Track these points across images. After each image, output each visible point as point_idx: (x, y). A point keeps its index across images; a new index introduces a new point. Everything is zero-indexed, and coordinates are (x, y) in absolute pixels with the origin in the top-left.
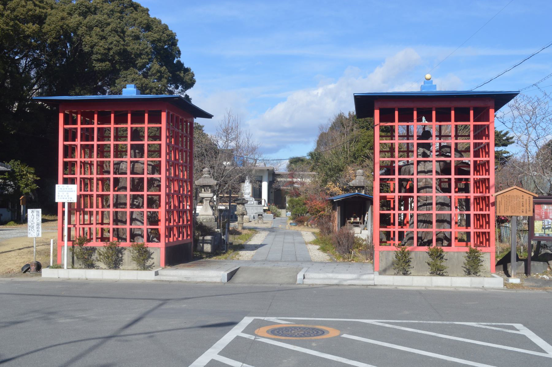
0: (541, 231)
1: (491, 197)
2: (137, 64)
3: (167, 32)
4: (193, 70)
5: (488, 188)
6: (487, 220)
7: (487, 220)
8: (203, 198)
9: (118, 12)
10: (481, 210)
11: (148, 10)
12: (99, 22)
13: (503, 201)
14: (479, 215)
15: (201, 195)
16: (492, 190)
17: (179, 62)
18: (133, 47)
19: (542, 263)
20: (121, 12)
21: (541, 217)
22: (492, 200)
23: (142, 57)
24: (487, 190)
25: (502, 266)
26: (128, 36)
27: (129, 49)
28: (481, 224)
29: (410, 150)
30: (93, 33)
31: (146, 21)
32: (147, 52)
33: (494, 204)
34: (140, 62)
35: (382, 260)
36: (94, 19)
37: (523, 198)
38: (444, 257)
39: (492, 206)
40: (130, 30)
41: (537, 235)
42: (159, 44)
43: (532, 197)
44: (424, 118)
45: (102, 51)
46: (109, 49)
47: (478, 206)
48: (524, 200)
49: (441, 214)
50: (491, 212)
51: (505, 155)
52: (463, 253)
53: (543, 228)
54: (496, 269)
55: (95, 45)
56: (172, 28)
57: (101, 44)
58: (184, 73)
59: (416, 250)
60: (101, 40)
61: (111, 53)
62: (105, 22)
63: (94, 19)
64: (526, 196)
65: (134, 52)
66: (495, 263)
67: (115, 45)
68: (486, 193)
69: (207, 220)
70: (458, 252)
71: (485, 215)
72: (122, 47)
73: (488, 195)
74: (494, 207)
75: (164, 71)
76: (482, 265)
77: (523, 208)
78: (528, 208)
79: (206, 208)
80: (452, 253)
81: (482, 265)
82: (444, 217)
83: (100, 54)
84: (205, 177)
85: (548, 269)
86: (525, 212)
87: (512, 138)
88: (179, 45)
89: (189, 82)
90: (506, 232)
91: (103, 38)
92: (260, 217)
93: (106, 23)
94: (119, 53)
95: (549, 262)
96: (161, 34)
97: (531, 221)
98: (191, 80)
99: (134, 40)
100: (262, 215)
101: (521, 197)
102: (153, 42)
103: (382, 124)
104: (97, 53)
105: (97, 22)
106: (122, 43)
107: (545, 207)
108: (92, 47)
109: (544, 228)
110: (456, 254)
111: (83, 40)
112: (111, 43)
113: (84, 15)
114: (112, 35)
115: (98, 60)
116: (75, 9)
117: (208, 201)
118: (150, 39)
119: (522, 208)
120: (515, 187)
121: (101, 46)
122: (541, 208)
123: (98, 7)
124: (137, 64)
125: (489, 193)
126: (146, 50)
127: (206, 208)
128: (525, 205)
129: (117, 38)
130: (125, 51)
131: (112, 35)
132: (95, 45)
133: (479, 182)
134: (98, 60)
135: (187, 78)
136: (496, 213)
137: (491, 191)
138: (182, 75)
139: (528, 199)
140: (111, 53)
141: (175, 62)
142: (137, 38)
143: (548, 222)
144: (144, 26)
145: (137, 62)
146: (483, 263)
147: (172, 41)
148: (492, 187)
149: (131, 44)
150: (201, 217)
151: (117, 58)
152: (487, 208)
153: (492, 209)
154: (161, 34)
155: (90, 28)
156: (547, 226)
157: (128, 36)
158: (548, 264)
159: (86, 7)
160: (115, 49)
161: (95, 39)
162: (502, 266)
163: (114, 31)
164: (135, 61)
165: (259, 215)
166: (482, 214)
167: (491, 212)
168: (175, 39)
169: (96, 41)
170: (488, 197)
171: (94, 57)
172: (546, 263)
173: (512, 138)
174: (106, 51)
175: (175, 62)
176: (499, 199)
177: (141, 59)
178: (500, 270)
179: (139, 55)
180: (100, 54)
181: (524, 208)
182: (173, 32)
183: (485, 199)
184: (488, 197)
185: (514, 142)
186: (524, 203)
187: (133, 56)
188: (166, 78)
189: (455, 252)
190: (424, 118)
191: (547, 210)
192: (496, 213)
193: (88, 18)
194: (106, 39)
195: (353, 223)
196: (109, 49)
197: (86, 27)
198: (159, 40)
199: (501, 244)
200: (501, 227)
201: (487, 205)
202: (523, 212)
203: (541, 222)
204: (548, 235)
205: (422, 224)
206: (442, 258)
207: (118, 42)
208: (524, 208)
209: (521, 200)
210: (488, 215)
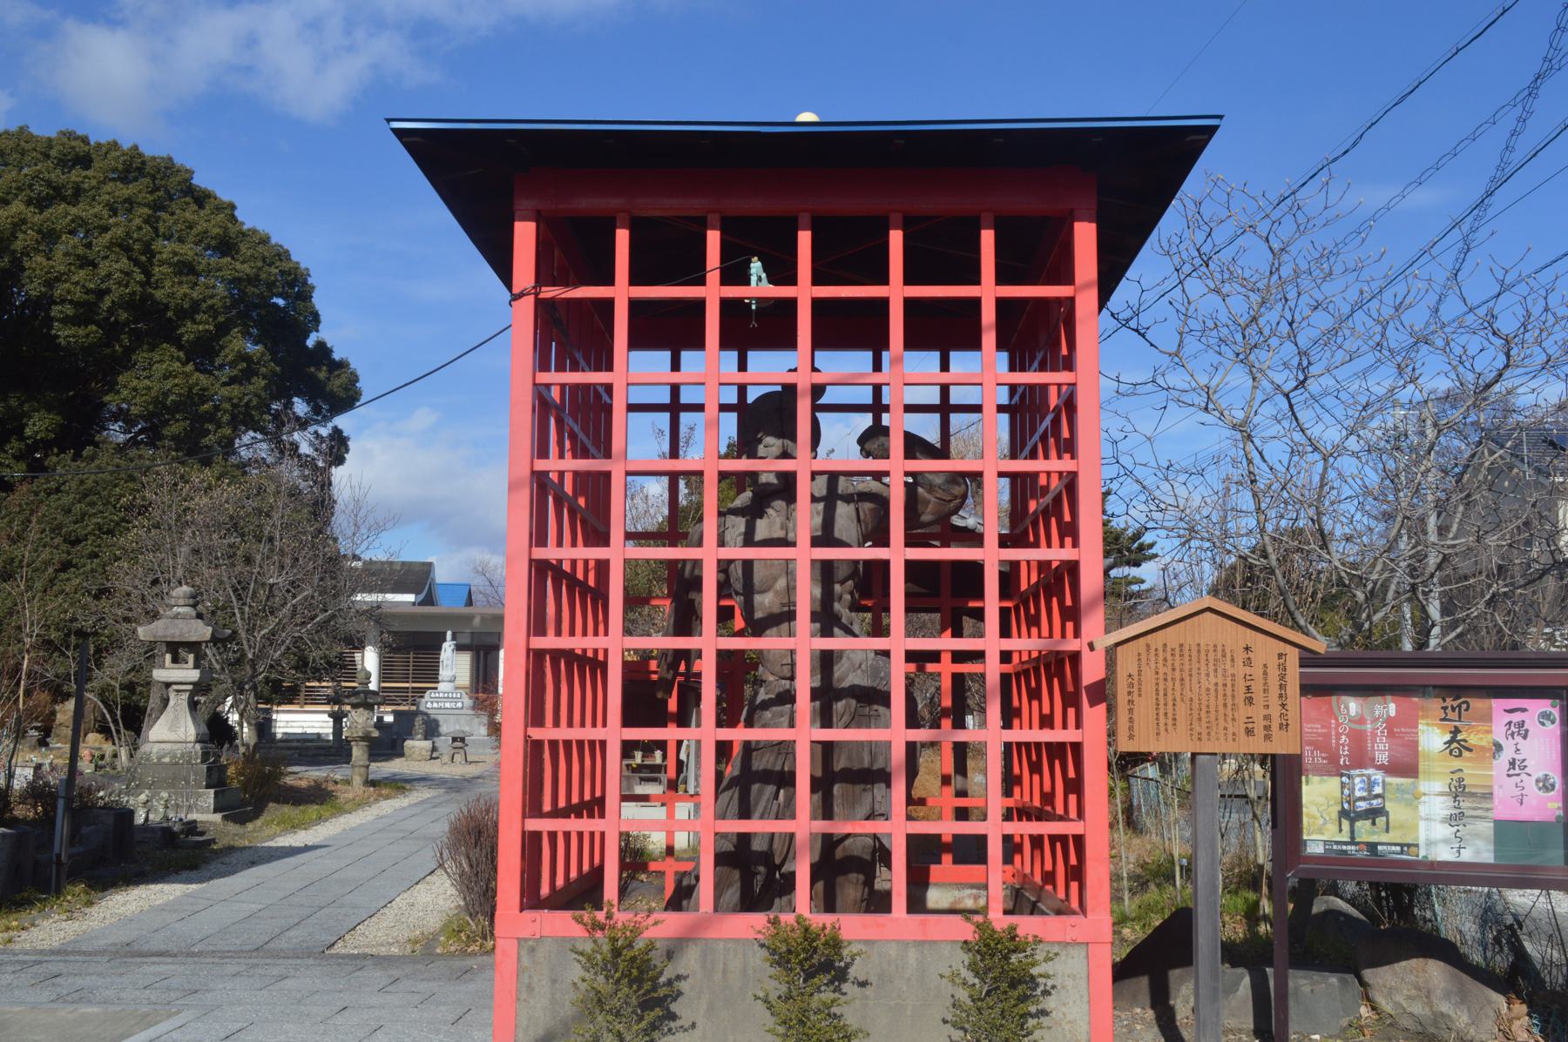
0: (1333, 827)
1: (1086, 656)
2: (182, 335)
3: (285, 266)
4: (354, 364)
5: (1072, 615)
6: (1072, 774)
7: (1072, 774)
8: (168, 685)
9: (145, 205)
10: (1046, 722)
11: (233, 207)
12: (80, 222)
13: (1148, 674)
14: (1038, 745)
15: (159, 675)
16: (1093, 622)
17: (321, 345)
18: (170, 290)
19: (1334, 979)
20: (157, 206)
21: (1333, 758)
22: (1092, 670)
23: (198, 317)
24: (1070, 625)
25: (1143, 982)
26: (162, 263)
27: (159, 294)
28: (1047, 788)
29: (667, 400)
30: (60, 249)
31: (216, 231)
32: (211, 307)
33: (1101, 693)
34: (189, 331)
35: (530, 988)
36: (67, 214)
37: (1248, 662)
38: (852, 972)
39: (1092, 704)
40: (165, 248)
41: (1315, 848)
42: (251, 290)
43: (1293, 655)
44: (756, 267)
45: (78, 295)
46: (101, 294)
47: (1035, 704)
48: (1257, 671)
49: (860, 744)
50: (1091, 732)
51: (1135, 588)
52: (946, 950)
53: (1343, 814)
54: (1116, 996)
55: (58, 279)
56: (302, 255)
57: (75, 278)
58: (330, 372)
59: (711, 934)
60: (81, 267)
61: (107, 303)
62: (97, 222)
63: (67, 214)
64: (1266, 650)
65: (172, 305)
66: (1107, 974)
67: (119, 284)
68: (1063, 636)
69: (175, 756)
70: (920, 944)
71: (1062, 745)
72: (138, 289)
73: (1071, 645)
74: (1102, 707)
75: (260, 359)
76: (1044, 1013)
77: (1250, 711)
78: (1275, 711)
79: (176, 718)
80: (893, 951)
81: (1044, 1013)
82: (873, 757)
83: (71, 302)
84: (176, 616)
85: (1364, 1011)
86: (1260, 732)
87: (1151, 546)
88: (319, 301)
89: (342, 394)
90: (1146, 793)
91: (87, 263)
92: (459, 744)
93: (99, 227)
94: (130, 304)
95: (1368, 974)
96: (260, 264)
97: (1285, 775)
98: (346, 389)
99: (180, 273)
100: (463, 740)
101: (1241, 656)
102: (236, 281)
103: (549, 292)
104: (63, 301)
105: (73, 221)
106: (140, 277)
107: (1353, 705)
108: (49, 284)
109: (1348, 815)
110: (912, 955)
111: (27, 265)
112: (109, 275)
113: (41, 203)
114: (113, 257)
115: (66, 321)
116: (18, 188)
117: (185, 696)
118: (227, 274)
119: (1243, 711)
120: (1208, 601)
121: (77, 283)
122: (1331, 713)
123: (86, 186)
124: (182, 335)
125: (1077, 634)
126: (210, 302)
127: (176, 718)
128: (1258, 697)
129: (124, 263)
130: (147, 297)
131: (113, 257)
132: (58, 279)
133: (1037, 670)
134: (66, 321)
135: (336, 384)
136: (1112, 734)
137: (1086, 627)
138: (322, 375)
139: (1273, 662)
140: (107, 303)
141: (310, 343)
142: (186, 269)
143: (1371, 784)
144: (213, 243)
145: (183, 330)
146: (1050, 1003)
147: (297, 285)
148: (1093, 604)
149: (168, 283)
150: (156, 748)
151: (124, 316)
152: (1071, 712)
153: (1094, 715)
154: (260, 264)
155: (50, 237)
156: (1362, 805)
157: (162, 263)
158: (1362, 983)
159: (49, 183)
160: (117, 292)
161: (59, 263)
162: (1143, 982)
163: (120, 246)
164: (178, 327)
165: (454, 740)
166: (1049, 745)
167: (1091, 732)
168: (305, 282)
169: (62, 268)
170: (1075, 657)
171: (56, 311)
172: (1350, 977)
173: (1151, 546)
174: (91, 298)
175: (310, 343)
176: (1127, 662)
177: (194, 322)
178: (1134, 1000)
179: (191, 311)
180: (71, 302)
181: (1257, 712)
182: (303, 266)
183: (1059, 666)
184: (1075, 657)
185: (1156, 556)
186: (1257, 687)
187: (170, 314)
188: (264, 377)
189: (904, 944)
190: (756, 267)
191: (1361, 720)
192: (1112, 734)
193: (46, 214)
194: (95, 266)
195: (640, 768)
196: (101, 294)
197: (39, 232)
198: (253, 280)
199: (1136, 841)
200: (1132, 780)
201: (1071, 700)
202: (1249, 732)
203: (1334, 783)
204: (1372, 847)
205: (771, 789)
206: (841, 976)
207: (127, 274)
208: (1257, 712)
209: (1241, 670)
210: (1077, 747)
